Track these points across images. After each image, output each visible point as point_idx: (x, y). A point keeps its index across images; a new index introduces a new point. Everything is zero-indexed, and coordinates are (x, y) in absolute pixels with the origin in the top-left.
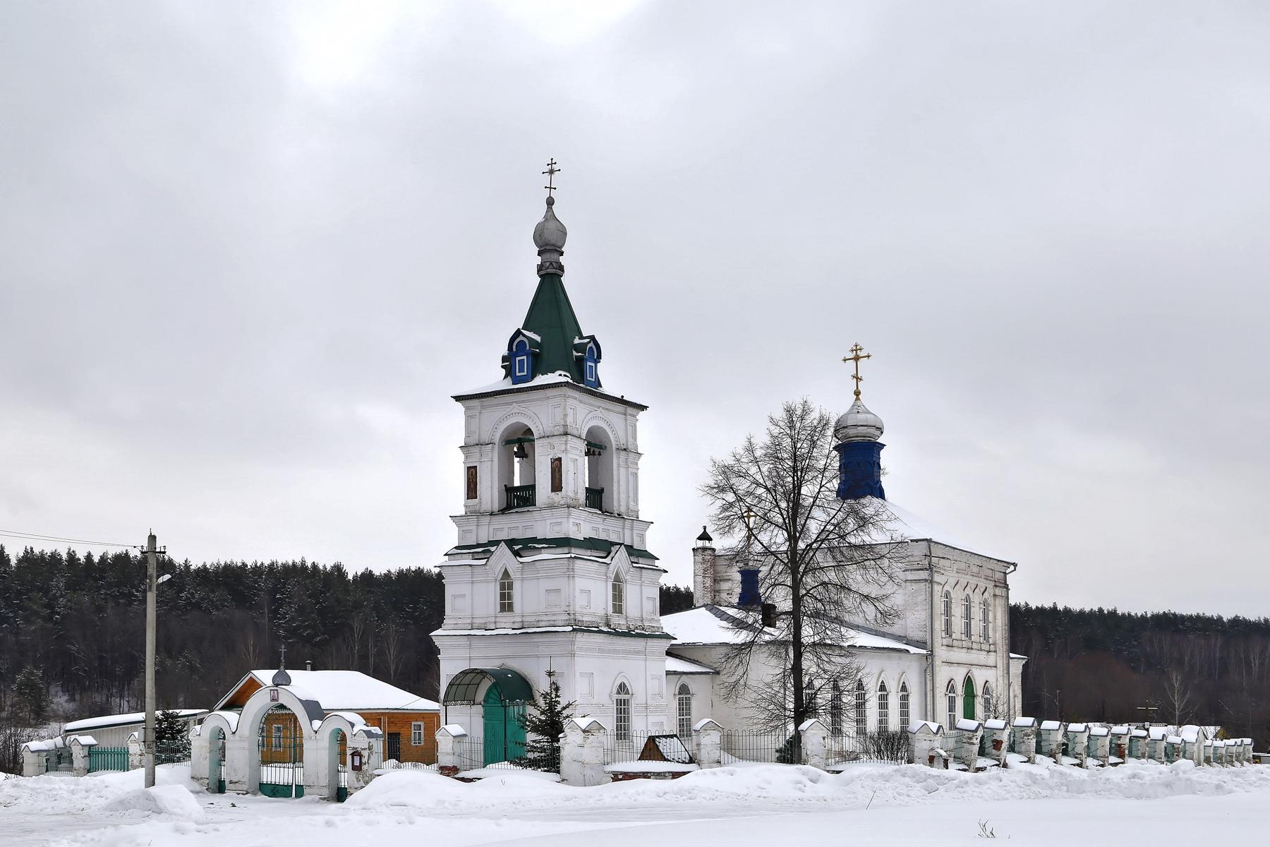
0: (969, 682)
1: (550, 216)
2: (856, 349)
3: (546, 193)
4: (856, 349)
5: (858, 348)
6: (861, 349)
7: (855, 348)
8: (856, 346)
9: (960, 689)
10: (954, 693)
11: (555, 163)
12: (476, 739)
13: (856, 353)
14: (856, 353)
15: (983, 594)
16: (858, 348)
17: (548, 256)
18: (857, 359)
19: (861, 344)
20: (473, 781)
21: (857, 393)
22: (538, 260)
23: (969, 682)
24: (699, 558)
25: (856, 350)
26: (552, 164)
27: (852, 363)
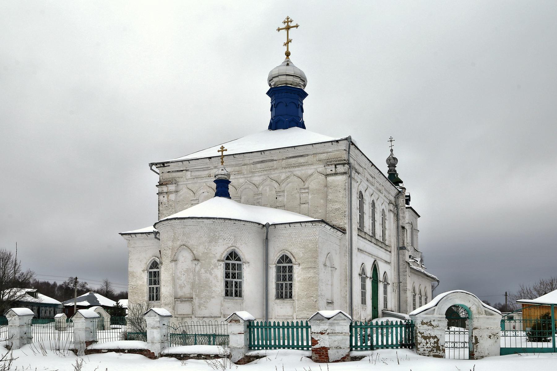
0: (375, 269)
1: (392, 154)
2: (288, 21)
3: (390, 148)
4: (288, 21)
5: (289, 20)
6: (291, 21)
7: (286, 20)
8: (288, 19)
9: (369, 273)
10: (364, 274)
11: (392, 138)
12: (171, 323)
13: (288, 24)
14: (288, 24)
15: (377, 200)
16: (289, 20)
17: (391, 168)
18: (288, 28)
19: (291, 17)
20: (101, 353)
21: (288, 54)
22: (388, 169)
23: (375, 269)
24: (548, 282)
25: (288, 22)
26: (391, 138)
27: (285, 32)
